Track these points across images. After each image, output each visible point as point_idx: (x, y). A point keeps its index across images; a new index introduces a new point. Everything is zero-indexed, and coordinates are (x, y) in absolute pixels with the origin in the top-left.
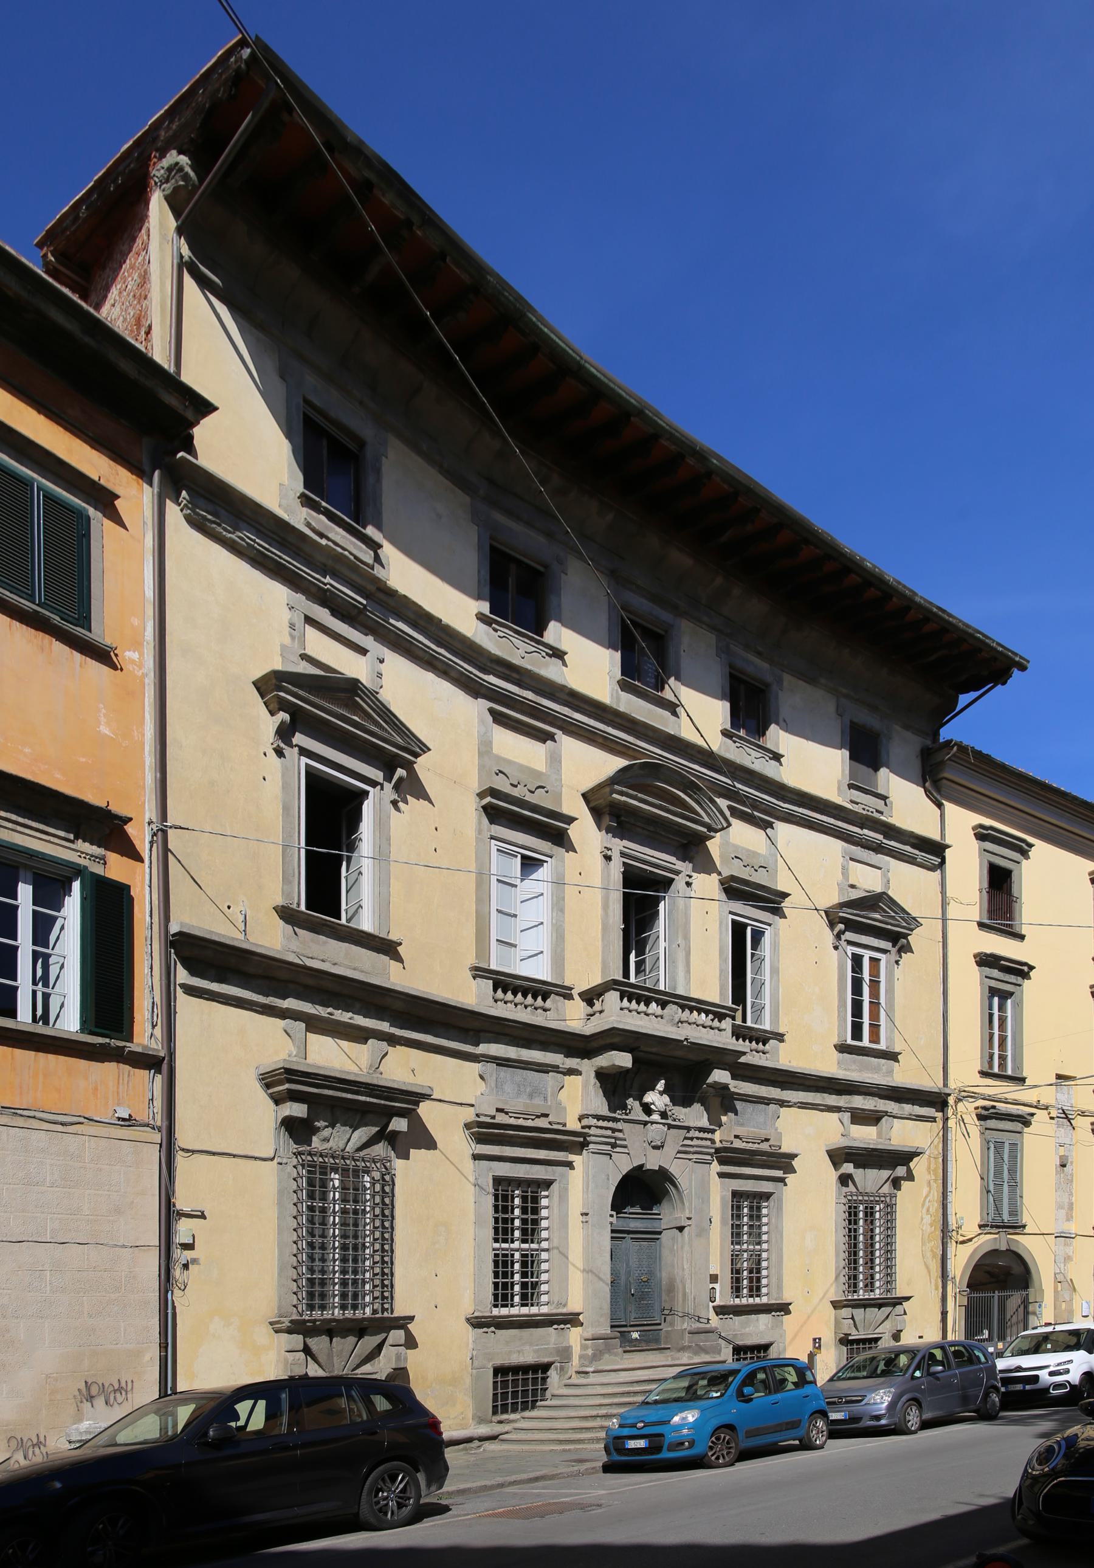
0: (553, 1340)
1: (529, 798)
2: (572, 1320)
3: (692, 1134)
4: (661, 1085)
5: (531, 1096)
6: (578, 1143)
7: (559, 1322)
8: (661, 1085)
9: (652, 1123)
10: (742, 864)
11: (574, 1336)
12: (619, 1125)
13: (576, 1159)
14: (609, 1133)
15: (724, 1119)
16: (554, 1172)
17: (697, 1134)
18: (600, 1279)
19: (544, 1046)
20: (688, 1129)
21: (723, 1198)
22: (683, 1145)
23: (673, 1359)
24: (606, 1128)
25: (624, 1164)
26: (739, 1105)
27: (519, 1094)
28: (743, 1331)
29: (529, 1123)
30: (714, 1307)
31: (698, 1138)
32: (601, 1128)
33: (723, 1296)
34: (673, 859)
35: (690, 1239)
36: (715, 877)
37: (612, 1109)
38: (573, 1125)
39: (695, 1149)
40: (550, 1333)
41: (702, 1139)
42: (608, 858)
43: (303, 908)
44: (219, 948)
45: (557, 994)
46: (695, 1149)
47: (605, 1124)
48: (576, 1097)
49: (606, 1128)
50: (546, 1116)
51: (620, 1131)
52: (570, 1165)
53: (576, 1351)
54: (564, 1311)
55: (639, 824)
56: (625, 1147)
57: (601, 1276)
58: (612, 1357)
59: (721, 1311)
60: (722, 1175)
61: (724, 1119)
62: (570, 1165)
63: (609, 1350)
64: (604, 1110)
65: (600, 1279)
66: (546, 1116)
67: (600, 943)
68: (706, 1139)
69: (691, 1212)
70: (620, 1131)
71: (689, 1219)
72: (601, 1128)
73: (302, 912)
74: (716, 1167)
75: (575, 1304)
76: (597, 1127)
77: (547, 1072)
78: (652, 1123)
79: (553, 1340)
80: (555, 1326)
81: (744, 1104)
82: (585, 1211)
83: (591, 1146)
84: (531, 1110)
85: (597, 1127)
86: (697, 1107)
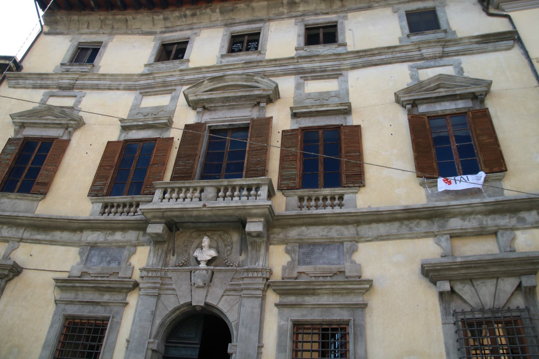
8: (206, 241)
16: (111, 311)
25: (171, 303)
27: (102, 261)
38: (136, 276)
74: (272, 298)
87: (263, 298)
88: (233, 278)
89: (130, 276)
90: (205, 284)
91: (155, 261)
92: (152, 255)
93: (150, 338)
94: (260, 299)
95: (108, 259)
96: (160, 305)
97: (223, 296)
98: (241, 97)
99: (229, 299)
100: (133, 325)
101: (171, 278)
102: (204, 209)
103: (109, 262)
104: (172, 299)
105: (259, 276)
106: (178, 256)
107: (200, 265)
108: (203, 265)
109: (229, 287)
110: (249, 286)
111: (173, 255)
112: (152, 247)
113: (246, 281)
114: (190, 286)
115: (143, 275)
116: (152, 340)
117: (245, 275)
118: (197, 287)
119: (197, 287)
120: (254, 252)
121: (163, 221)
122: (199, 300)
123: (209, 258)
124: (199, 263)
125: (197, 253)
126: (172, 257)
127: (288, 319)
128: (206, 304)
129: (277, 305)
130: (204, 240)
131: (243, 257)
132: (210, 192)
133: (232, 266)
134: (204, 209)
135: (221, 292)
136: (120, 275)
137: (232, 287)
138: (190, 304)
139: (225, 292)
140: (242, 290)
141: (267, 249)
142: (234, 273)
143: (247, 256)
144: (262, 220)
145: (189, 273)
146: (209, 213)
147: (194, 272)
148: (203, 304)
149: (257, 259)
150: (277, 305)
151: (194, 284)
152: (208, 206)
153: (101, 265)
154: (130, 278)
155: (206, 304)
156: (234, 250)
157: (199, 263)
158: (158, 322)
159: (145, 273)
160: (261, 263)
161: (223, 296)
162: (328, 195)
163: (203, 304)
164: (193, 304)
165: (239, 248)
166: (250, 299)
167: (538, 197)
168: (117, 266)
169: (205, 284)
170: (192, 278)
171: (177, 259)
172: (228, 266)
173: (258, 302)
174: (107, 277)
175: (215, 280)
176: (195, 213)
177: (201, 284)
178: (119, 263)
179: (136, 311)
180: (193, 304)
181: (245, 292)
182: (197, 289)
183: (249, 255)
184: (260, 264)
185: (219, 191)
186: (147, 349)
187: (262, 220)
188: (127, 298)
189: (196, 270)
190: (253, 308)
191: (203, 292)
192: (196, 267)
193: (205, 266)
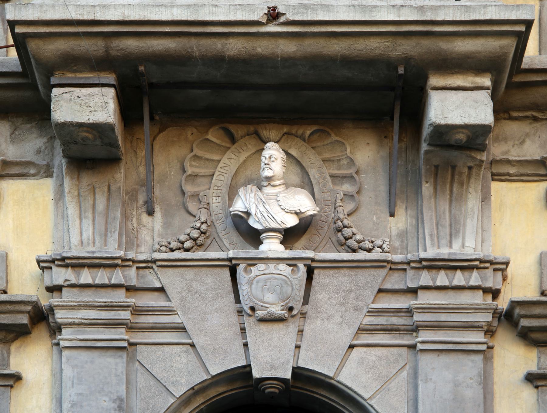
83: (66, 333)
87: (487, 353)
88: (380, 291)
90: (291, 309)
91: (88, 232)
92: (72, 210)
94: (479, 358)
96: (142, 379)
99: (373, 358)
101: (161, 290)
102: (272, 28)
104: (180, 358)
105: (472, 283)
106: (166, 214)
107: (262, 247)
108: (272, 246)
109: (369, 320)
110: (443, 317)
111: (151, 213)
112: (67, 182)
113: (426, 299)
114: (234, 317)
115: (60, 281)
117: (425, 278)
118: (263, 320)
119: (263, 320)
120: (444, 205)
121: (111, 78)
122: (272, 358)
123: (292, 221)
124: (254, 237)
125: (245, 201)
126: (145, 218)
128: (297, 372)
129: (532, 379)
130: (266, 153)
131: (401, 221)
133: (369, 251)
134: (272, 28)
135: (346, 336)
137: (381, 321)
138: (245, 372)
140: (415, 329)
141: (486, 198)
142: (384, 272)
143: (419, 219)
144: (487, 81)
145: (226, 273)
146: (288, 48)
148: (288, 375)
149: (455, 231)
150: (532, 379)
151: (253, 309)
152: (291, 17)
155: (297, 372)
156: (366, 198)
157: (254, 237)
160: (470, 243)
161: (352, 347)
163: (288, 375)
164: (256, 374)
165: (383, 188)
166: (445, 359)
169: (291, 309)
170: (243, 289)
171: (166, 225)
172: (354, 251)
173: (472, 365)
175: (319, 294)
176: (235, 47)
177: (277, 310)
180: (256, 374)
181: (425, 335)
182: (264, 327)
183: (428, 215)
184: (467, 247)
187: (487, 81)
188: (12, 361)
189: (252, 262)
190: (457, 385)
191: (285, 334)
192: (252, 253)
193: (282, 247)
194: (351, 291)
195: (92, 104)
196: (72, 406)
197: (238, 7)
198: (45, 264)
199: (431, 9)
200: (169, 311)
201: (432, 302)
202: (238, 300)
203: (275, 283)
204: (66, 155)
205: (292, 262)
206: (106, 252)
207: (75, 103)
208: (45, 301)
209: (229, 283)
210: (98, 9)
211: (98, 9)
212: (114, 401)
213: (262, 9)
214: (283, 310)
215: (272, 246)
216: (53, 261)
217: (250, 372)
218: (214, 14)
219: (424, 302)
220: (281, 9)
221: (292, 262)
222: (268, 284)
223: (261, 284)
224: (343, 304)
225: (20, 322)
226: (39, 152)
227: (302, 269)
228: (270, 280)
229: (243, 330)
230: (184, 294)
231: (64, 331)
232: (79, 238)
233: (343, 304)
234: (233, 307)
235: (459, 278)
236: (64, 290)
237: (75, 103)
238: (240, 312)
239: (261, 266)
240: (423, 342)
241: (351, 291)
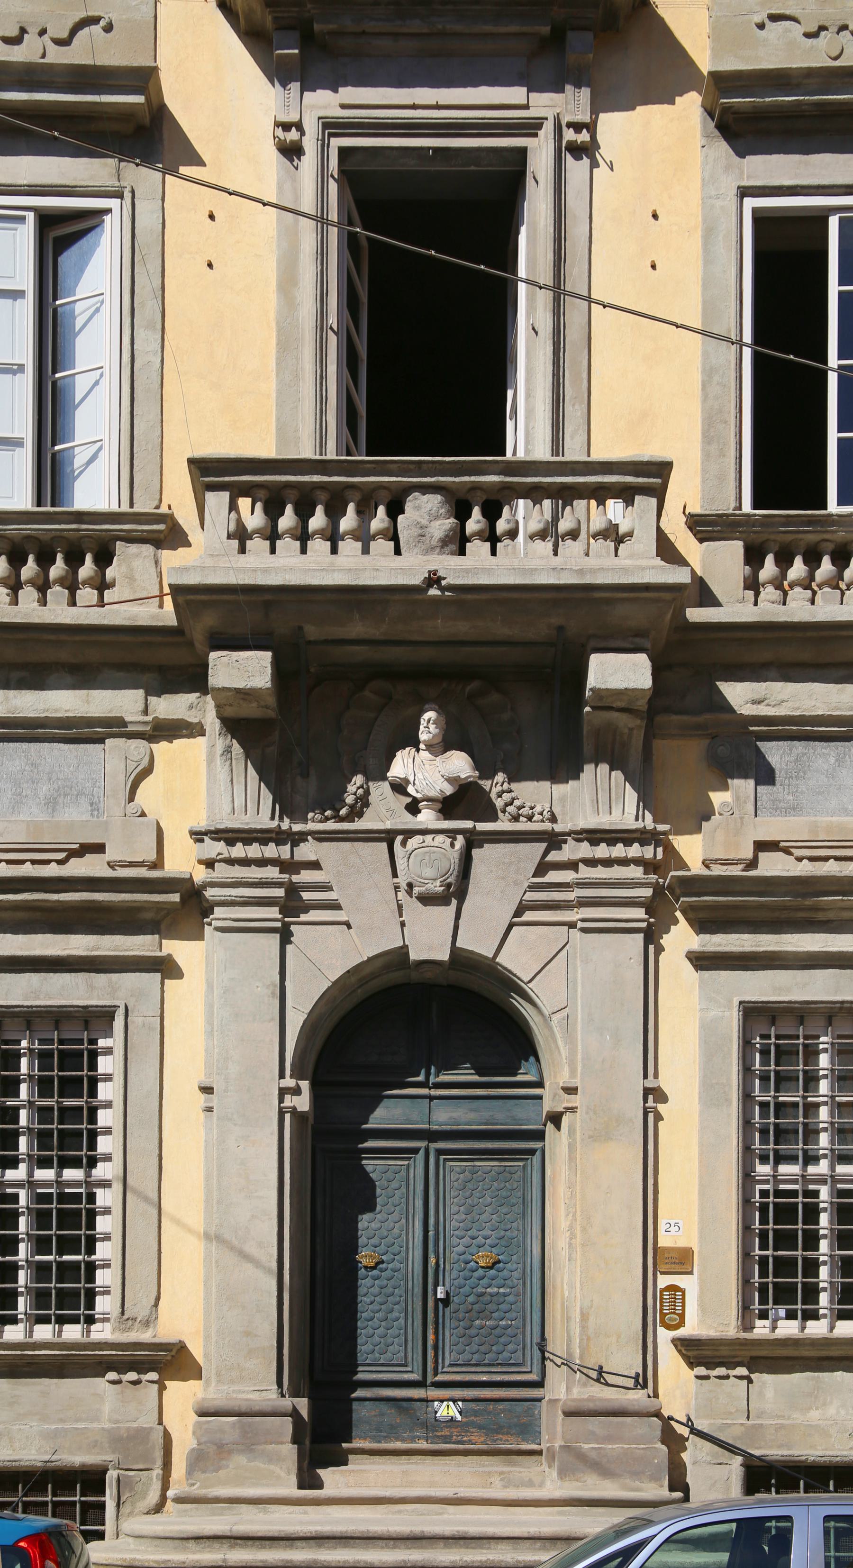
0: (107, 1408)
1: (57, 56)
2: (171, 1361)
3: (570, 851)
4: (429, 724)
5: (52, 803)
6: (189, 908)
7: (122, 1366)
8: (429, 724)
9: (424, 832)
10: (797, 30)
11: (181, 1397)
12: (307, 851)
13: (178, 949)
14: (272, 873)
15: (718, 798)
17: (585, 850)
18: (246, 1257)
19: (83, 676)
20: (554, 840)
21: (708, 1030)
22: (533, 887)
23: (508, 1483)
24: (262, 862)
25: (326, 956)
26: (776, 753)
28: (798, 1418)
29: (52, 871)
30: (674, 1341)
31: (591, 862)
32: (245, 862)
33: (710, 1304)
34: (516, 94)
35: (572, 1147)
36: (691, 104)
37: (286, 806)
38: (182, 860)
39: (571, 896)
40: (100, 1394)
41: (608, 863)
42: (291, 151)
43: (747, 507)
44: (515, 595)
45: (130, 539)
46: (571, 896)
47: (254, 851)
48: (189, 791)
49: (262, 862)
50: (99, 848)
51: (315, 865)
52: (167, 968)
53: (184, 1443)
54: (146, 1336)
55: (370, 26)
56: (335, 906)
57: (251, 1248)
58: (259, 1464)
59: (699, 1353)
60: (702, 961)
61: (718, 798)
62: (167, 968)
63: (249, 1444)
64: (262, 814)
65: (246, 1257)
66: (99, 848)
67: (270, 386)
68: (624, 862)
69: (573, 1073)
70: (315, 865)
71: (571, 1090)
72: (245, 862)
73: (748, 515)
74: (681, 938)
75: (181, 1318)
76: (231, 862)
77: (101, 740)
78: (424, 832)
79: (107, 1408)
80: (112, 1375)
81: (799, 747)
82: (207, 1084)
83: (218, 912)
84: (47, 838)
85: (231, 862)
86: (597, 777)
89: (152, 856)
93: (282, 1076)
95: (44, 789)
97: (511, 926)
98: (515, 34)
100: (210, 1034)
103: (52, 803)
111: (306, 775)
116: (289, 1082)
122: (429, 939)
127: (731, 1001)
132: (425, 513)
136: (111, 854)
138: (403, 951)
139: (518, 913)
145: (384, 845)
147: (404, 844)
153: (23, 817)
154: (158, 864)
158: (295, 1021)
159: (215, 848)
161: (511, 926)
162: (747, 1177)
167: (851, 1048)
168: (86, 817)
174: (60, 862)
178: (94, 807)
179: (210, 986)
180: (413, 956)
185: (462, 513)
186: (281, 1113)
194: (511, 863)
195: (250, 669)
196: (224, 993)
197: (399, 571)
198: (198, 836)
199: (590, 572)
200: (327, 887)
201: (595, 876)
202: (395, 875)
203: (433, 856)
204: (220, 717)
205: (452, 834)
206: (260, 823)
207: (233, 667)
208: (200, 875)
209: (386, 856)
210: (259, 573)
211: (259, 573)
212: (268, 987)
213: (423, 573)
214: (441, 886)
215: (427, 817)
216: (206, 833)
217: (407, 953)
218: (375, 578)
219: (586, 876)
220: (441, 573)
221: (452, 834)
222: (427, 858)
223: (419, 858)
224: (503, 878)
225: (172, 900)
226: (191, 707)
227: (460, 841)
228: (430, 857)
229: (400, 907)
230: (340, 868)
231: (216, 909)
232: (231, 806)
233: (503, 878)
234: (390, 881)
235: (619, 851)
236: (216, 864)
237: (233, 667)
238: (397, 888)
239: (418, 838)
240: (583, 920)
241: (511, 863)
